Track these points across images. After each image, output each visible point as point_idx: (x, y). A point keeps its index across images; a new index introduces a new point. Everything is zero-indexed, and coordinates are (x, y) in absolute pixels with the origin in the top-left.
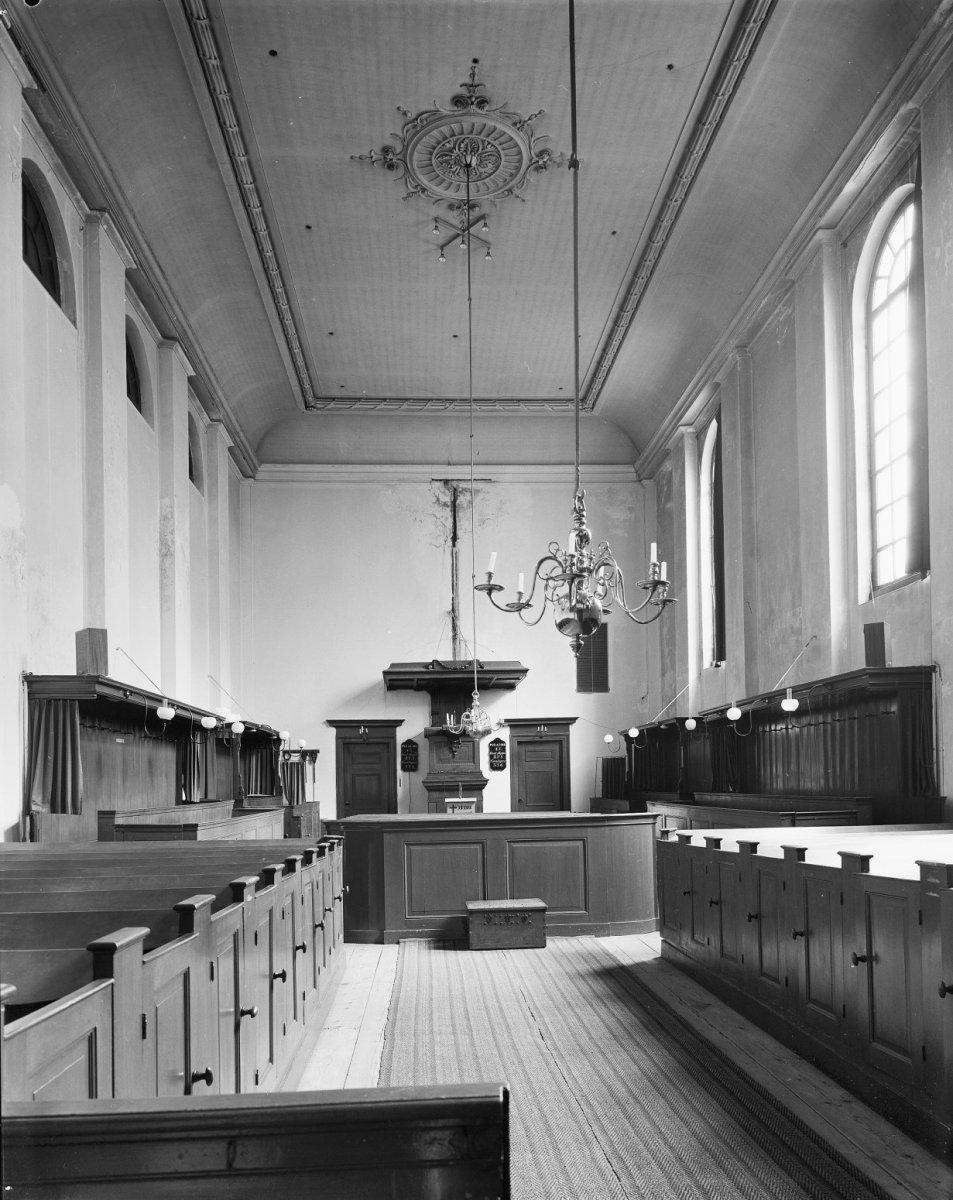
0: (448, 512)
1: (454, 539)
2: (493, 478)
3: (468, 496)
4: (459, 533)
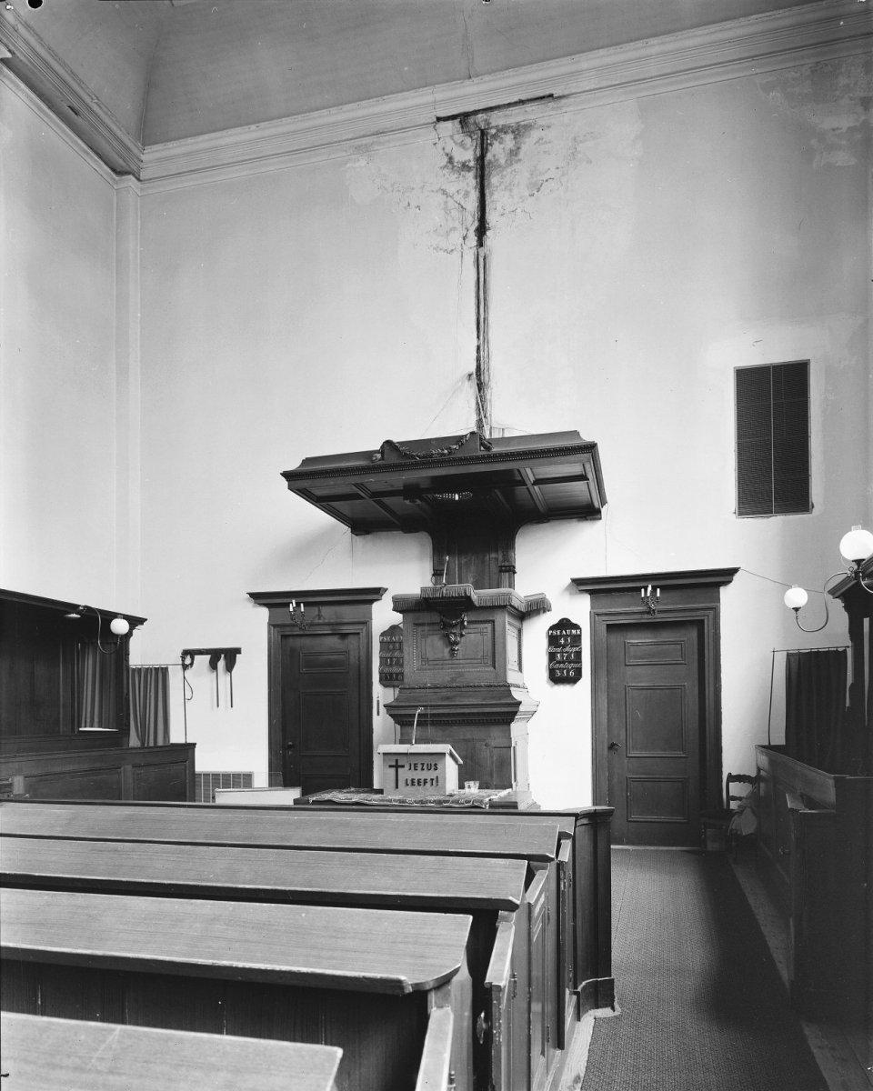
0: (470, 180)
1: (482, 230)
2: (556, 93)
3: (509, 141)
4: (492, 218)
